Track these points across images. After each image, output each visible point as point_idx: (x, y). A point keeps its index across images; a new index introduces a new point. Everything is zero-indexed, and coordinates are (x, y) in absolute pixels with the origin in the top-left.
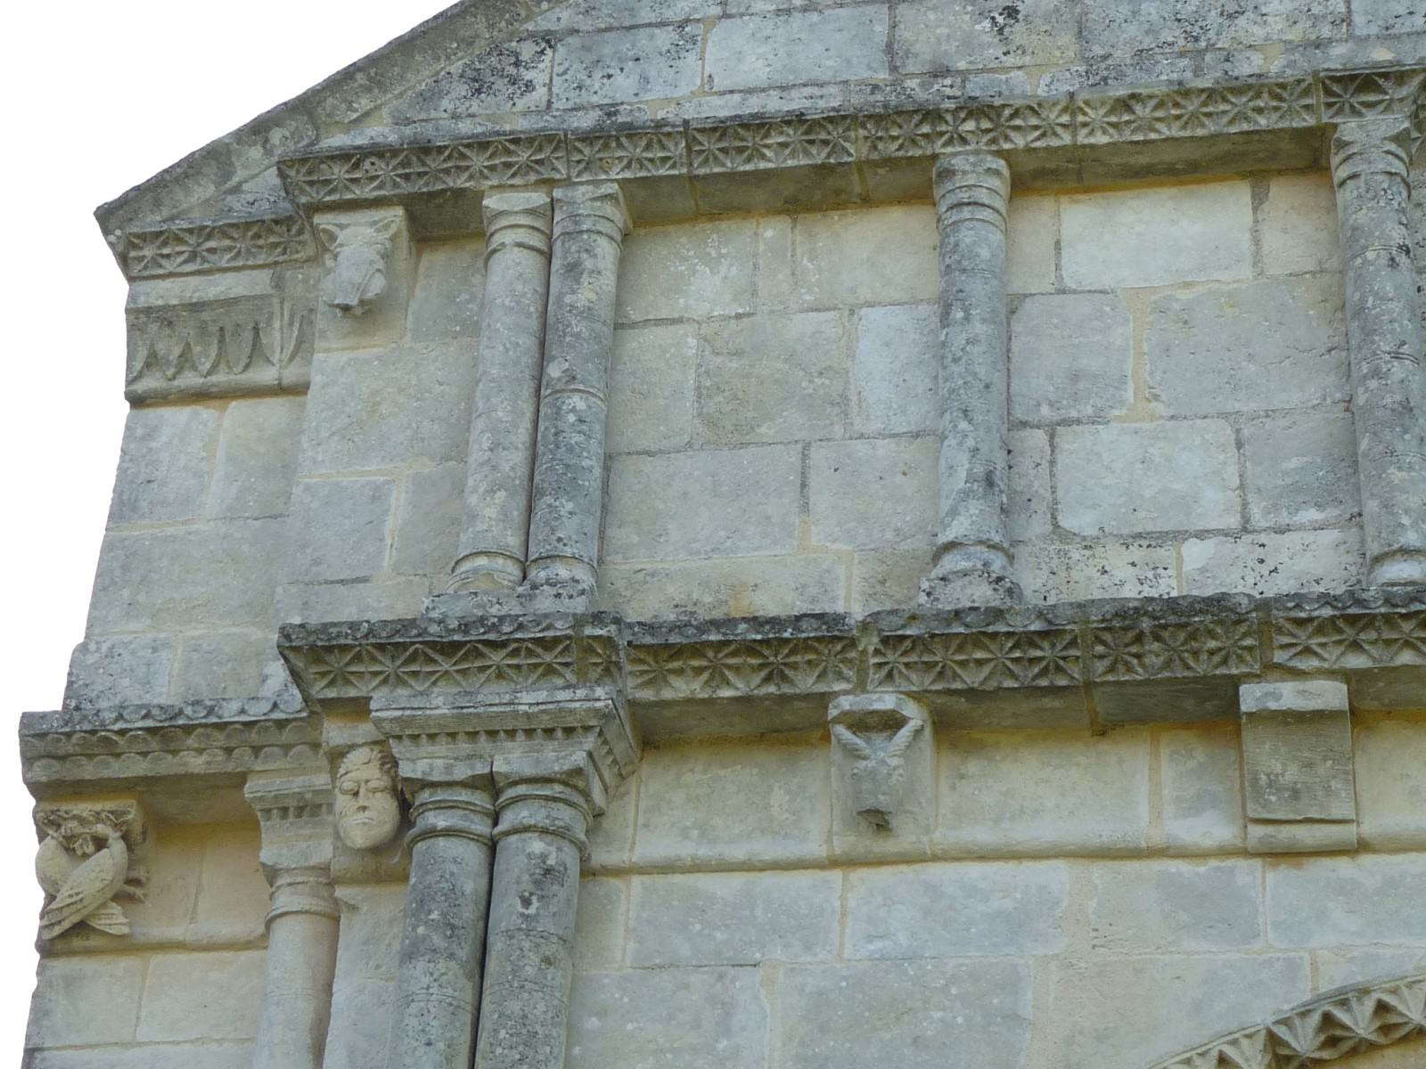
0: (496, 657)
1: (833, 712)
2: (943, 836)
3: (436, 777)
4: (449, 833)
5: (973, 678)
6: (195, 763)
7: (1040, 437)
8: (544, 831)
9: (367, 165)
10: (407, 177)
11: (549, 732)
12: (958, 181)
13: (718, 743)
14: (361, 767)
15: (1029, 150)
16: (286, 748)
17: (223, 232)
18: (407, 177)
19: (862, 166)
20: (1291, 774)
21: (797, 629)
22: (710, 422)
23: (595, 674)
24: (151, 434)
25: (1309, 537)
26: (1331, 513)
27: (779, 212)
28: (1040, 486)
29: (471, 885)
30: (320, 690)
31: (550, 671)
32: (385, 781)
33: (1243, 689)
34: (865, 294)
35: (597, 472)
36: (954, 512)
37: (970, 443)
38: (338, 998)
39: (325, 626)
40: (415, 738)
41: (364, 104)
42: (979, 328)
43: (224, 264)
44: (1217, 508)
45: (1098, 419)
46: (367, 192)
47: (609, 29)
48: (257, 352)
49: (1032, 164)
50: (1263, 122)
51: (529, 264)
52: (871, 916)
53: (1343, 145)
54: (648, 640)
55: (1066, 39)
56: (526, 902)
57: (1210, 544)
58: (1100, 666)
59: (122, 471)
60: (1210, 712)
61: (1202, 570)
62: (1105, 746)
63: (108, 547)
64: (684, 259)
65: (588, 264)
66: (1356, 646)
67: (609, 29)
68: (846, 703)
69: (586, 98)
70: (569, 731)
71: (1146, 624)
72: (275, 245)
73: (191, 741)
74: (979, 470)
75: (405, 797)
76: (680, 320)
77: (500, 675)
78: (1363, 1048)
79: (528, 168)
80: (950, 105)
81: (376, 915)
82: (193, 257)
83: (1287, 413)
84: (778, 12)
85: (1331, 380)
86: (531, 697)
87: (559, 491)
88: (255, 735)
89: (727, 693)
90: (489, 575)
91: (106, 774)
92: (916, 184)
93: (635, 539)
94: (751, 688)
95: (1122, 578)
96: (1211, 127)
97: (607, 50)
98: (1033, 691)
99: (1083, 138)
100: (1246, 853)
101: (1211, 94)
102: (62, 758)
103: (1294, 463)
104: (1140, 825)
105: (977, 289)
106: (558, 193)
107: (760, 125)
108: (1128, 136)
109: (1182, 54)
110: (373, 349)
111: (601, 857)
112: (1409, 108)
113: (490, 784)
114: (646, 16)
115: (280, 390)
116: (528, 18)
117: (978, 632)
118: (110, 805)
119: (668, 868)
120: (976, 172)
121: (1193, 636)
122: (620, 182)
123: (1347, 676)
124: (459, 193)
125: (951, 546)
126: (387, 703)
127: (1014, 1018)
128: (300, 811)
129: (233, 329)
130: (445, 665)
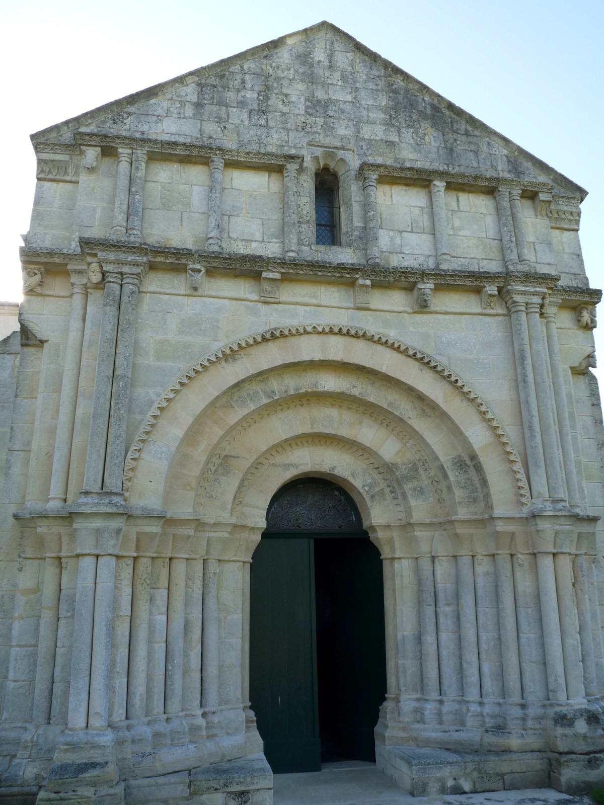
0: (124, 249)
1: (188, 268)
2: (206, 293)
3: (110, 271)
4: (113, 282)
5: (215, 265)
6: (57, 260)
7: (226, 218)
8: (132, 284)
9: (93, 137)
10: (102, 142)
11: (134, 265)
12: (215, 163)
13: (164, 270)
14: (95, 267)
15: (229, 159)
16: (77, 260)
17: (59, 145)
18: (102, 142)
19: (196, 156)
20: (269, 289)
21: (183, 251)
22: (163, 204)
23: (143, 254)
24: (42, 187)
25: (274, 244)
26: (278, 240)
27: (177, 162)
28: (226, 227)
29: (118, 293)
30: (87, 250)
31: (134, 253)
32: (100, 270)
33: (263, 273)
34: (194, 182)
35: (522, 471)
36: (212, 231)
37: (215, 218)
38: (88, 311)
39: (89, 238)
40: (107, 263)
41: (89, 121)
42: (218, 195)
43: (59, 152)
44: (258, 236)
45: (238, 216)
46: (93, 143)
47: (143, 114)
48: (66, 173)
49: (229, 162)
50: (273, 162)
51: (128, 165)
52: (192, 306)
53: (287, 169)
54: (154, 249)
55: (235, 135)
56: (129, 298)
57: (257, 243)
58: (238, 265)
59: (36, 195)
60: (256, 276)
61: (255, 248)
62: (236, 279)
63: (34, 211)
64: (158, 169)
65: (140, 168)
66: (283, 268)
67: (143, 114)
68: (191, 266)
69: (137, 129)
70: (138, 265)
71: (247, 259)
72: (70, 150)
73: (56, 256)
74: (217, 224)
75: (104, 274)
76: (157, 182)
77: (124, 252)
78: (277, 338)
79: (128, 144)
80: (215, 147)
81: (96, 297)
82: (52, 149)
83: (272, 220)
84: (178, 118)
85: (280, 215)
86: (131, 258)
87: (134, 215)
88: (70, 256)
89: (168, 261)
90: (121, 231)
91: (37, 260)
92: (206, 161)
93: (148, 226)
94: (171, 260)
95: (242, 249)
96: (263, 161)
97: (142, 119)
98: (225, 268)
99: (239, 159)
100: (260, 302)
101: (264, 155)
102: (28, 256)
103: (272, 230)
104: (241, 295)
105: (218, 187)
106: (134, 151)
107: (176, 144)
108: (248, 160)
109: (257, 143)
110: (93, 177)
111: (141, 290)
112: (299, 164)
113: (122, 273)
114: (150, 113)
115: (71, 182)
116: (126, 108)
117: (217, 256)
118: (37, 266)
119: (154, 293)
120: (218, 162)
121: (255, 262)
122: (148, 151)
123: (281, 273)
124: (113, 147)
125: (211, 238)
126: (101, 255)
127: (218, 327)
128: (79, 272)
129: (61, 167)
130: (113, 249)
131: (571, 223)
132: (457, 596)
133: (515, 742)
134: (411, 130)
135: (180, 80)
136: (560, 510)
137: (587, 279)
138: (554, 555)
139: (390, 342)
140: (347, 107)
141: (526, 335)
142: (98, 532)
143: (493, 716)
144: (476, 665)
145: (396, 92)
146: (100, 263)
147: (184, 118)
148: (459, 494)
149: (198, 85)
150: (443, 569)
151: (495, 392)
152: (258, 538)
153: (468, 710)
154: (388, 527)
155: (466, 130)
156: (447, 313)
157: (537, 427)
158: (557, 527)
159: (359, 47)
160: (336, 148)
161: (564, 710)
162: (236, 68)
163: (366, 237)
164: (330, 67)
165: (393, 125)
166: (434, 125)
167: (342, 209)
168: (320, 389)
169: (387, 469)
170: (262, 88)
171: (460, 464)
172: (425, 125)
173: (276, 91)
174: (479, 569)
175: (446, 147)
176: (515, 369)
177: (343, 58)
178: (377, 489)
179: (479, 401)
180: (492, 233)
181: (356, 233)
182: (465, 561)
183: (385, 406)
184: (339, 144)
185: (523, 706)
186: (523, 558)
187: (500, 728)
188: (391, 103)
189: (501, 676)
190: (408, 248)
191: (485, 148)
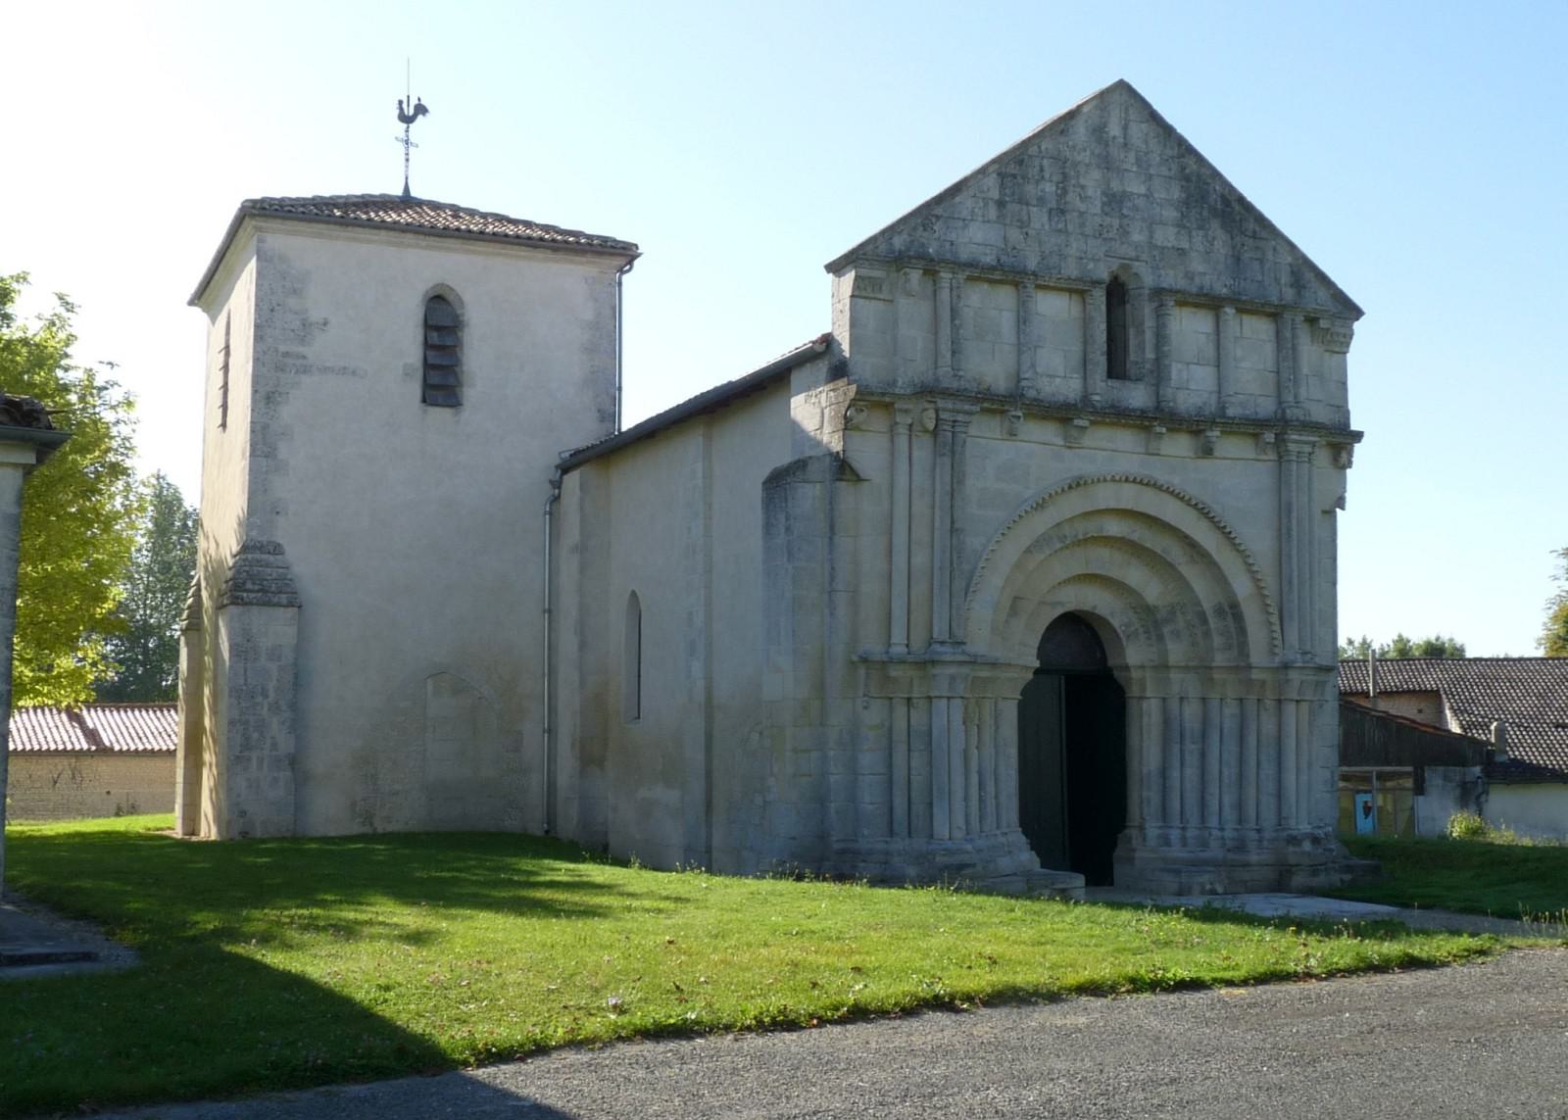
14: (931, 414)
35: (1278, 622)
114: (956, 216)
126: (941, 403)
131: (1339, 342)
132: (1204, 735)
133: (1254, 858)
134: (1201, 233)
135: (982, 171)
136: (1308, 662)
137: (1348, 412)
138: (1297, 701)
139: (1177, 491)
140: (1140, 202)
141: (1294, 487)
142: (953, 678)
143: (1233, 839)
144: (1217, 797)
145: (1187, 179)
146: (937, 411)
147: (988, 222)
148: (1217, 641)
149: (999, 174)
150: (1191, 712)
151: (1259, 540)
152: (1030, 676)
153: (1210, 834)
154: (1142, 667)
155: (1255, 232)
156: (1225, 459)
157: (1295, 581)
158: (1304, 678)
159: (1154, 117)
160: (1131, 259)
161: (1295, 833)
162: (1033, 150)
163: (1159, 375)
164: (1126, 145)
165: (1185, 227)
166: (1224, 226)
167: (1132, 332)
168: (1105, 534)
169: (1147, 611)
170: (1060, 177)
171: (1220, 612)
172: (1215, 227)
173: (1073, 182)
174: (1227, 711)
175: (1233, 256)
176: (1280, 519)
177: (1138, 131)
178: (1132, 629)
179: (1248, 553)
180: (1270, 364)
181: (1148, 366)
182: (1215, 704)
183: (1159, 552)
184: (1133, 254)
185: (1259, 831)
186: (1269, 703)
187: (1240, 846)
188: (1183, 195)
189: (1240, 806)
190: (1192, 384)
191: (1270, 255)
